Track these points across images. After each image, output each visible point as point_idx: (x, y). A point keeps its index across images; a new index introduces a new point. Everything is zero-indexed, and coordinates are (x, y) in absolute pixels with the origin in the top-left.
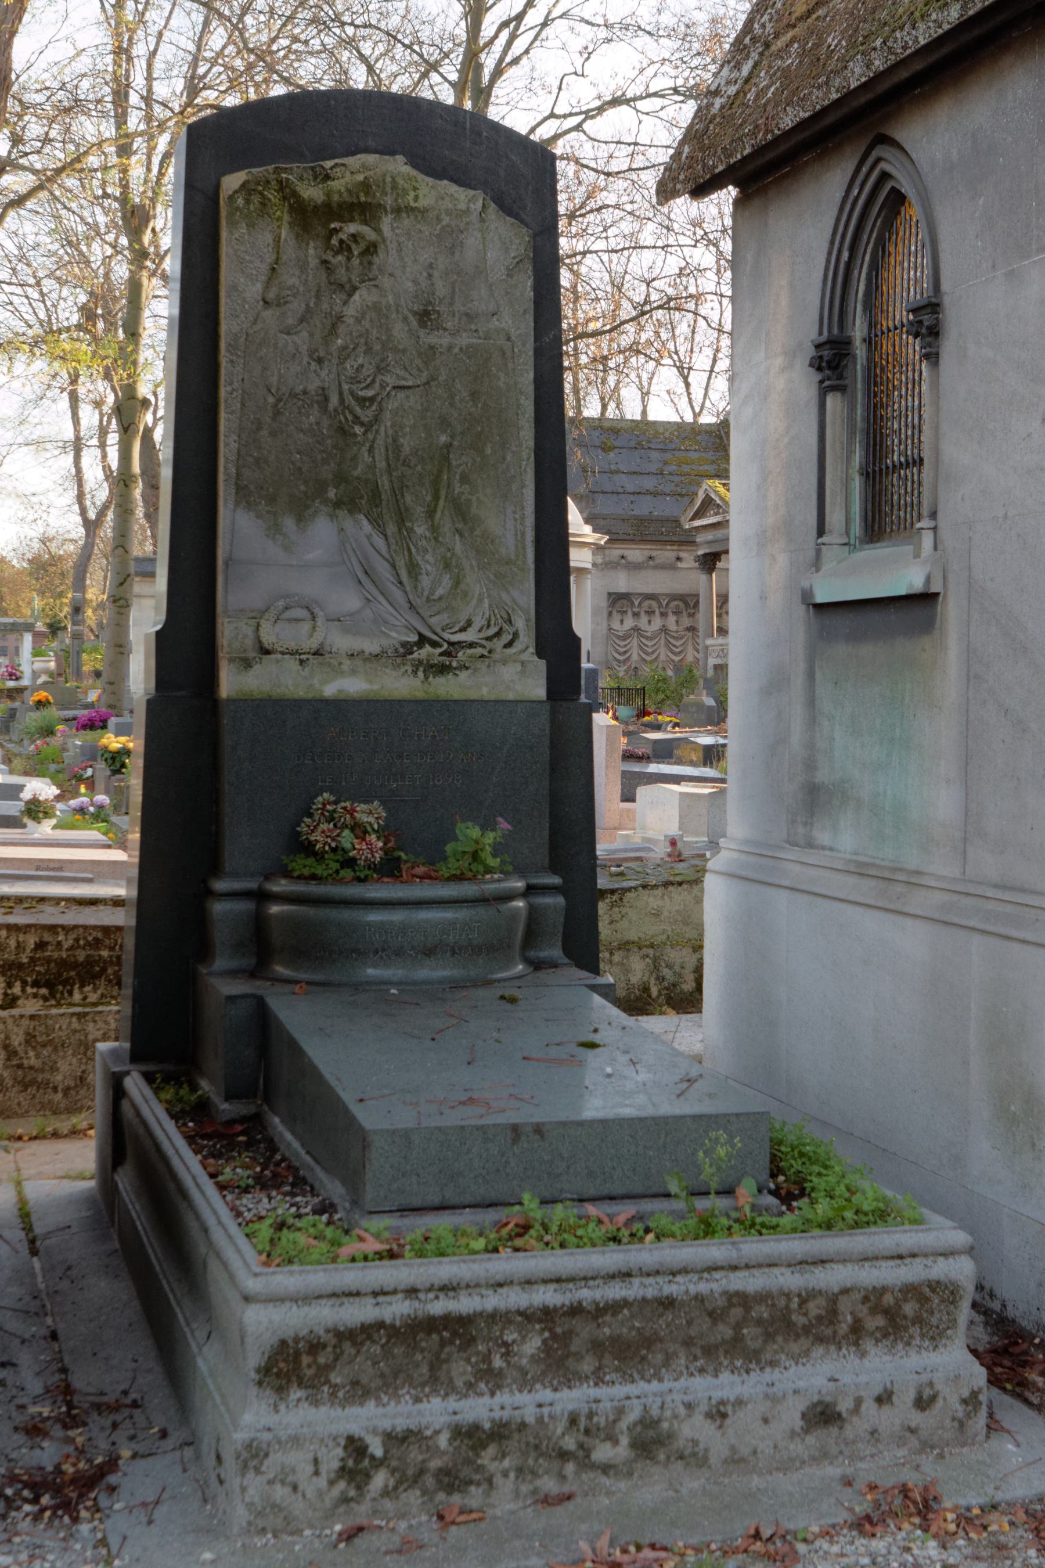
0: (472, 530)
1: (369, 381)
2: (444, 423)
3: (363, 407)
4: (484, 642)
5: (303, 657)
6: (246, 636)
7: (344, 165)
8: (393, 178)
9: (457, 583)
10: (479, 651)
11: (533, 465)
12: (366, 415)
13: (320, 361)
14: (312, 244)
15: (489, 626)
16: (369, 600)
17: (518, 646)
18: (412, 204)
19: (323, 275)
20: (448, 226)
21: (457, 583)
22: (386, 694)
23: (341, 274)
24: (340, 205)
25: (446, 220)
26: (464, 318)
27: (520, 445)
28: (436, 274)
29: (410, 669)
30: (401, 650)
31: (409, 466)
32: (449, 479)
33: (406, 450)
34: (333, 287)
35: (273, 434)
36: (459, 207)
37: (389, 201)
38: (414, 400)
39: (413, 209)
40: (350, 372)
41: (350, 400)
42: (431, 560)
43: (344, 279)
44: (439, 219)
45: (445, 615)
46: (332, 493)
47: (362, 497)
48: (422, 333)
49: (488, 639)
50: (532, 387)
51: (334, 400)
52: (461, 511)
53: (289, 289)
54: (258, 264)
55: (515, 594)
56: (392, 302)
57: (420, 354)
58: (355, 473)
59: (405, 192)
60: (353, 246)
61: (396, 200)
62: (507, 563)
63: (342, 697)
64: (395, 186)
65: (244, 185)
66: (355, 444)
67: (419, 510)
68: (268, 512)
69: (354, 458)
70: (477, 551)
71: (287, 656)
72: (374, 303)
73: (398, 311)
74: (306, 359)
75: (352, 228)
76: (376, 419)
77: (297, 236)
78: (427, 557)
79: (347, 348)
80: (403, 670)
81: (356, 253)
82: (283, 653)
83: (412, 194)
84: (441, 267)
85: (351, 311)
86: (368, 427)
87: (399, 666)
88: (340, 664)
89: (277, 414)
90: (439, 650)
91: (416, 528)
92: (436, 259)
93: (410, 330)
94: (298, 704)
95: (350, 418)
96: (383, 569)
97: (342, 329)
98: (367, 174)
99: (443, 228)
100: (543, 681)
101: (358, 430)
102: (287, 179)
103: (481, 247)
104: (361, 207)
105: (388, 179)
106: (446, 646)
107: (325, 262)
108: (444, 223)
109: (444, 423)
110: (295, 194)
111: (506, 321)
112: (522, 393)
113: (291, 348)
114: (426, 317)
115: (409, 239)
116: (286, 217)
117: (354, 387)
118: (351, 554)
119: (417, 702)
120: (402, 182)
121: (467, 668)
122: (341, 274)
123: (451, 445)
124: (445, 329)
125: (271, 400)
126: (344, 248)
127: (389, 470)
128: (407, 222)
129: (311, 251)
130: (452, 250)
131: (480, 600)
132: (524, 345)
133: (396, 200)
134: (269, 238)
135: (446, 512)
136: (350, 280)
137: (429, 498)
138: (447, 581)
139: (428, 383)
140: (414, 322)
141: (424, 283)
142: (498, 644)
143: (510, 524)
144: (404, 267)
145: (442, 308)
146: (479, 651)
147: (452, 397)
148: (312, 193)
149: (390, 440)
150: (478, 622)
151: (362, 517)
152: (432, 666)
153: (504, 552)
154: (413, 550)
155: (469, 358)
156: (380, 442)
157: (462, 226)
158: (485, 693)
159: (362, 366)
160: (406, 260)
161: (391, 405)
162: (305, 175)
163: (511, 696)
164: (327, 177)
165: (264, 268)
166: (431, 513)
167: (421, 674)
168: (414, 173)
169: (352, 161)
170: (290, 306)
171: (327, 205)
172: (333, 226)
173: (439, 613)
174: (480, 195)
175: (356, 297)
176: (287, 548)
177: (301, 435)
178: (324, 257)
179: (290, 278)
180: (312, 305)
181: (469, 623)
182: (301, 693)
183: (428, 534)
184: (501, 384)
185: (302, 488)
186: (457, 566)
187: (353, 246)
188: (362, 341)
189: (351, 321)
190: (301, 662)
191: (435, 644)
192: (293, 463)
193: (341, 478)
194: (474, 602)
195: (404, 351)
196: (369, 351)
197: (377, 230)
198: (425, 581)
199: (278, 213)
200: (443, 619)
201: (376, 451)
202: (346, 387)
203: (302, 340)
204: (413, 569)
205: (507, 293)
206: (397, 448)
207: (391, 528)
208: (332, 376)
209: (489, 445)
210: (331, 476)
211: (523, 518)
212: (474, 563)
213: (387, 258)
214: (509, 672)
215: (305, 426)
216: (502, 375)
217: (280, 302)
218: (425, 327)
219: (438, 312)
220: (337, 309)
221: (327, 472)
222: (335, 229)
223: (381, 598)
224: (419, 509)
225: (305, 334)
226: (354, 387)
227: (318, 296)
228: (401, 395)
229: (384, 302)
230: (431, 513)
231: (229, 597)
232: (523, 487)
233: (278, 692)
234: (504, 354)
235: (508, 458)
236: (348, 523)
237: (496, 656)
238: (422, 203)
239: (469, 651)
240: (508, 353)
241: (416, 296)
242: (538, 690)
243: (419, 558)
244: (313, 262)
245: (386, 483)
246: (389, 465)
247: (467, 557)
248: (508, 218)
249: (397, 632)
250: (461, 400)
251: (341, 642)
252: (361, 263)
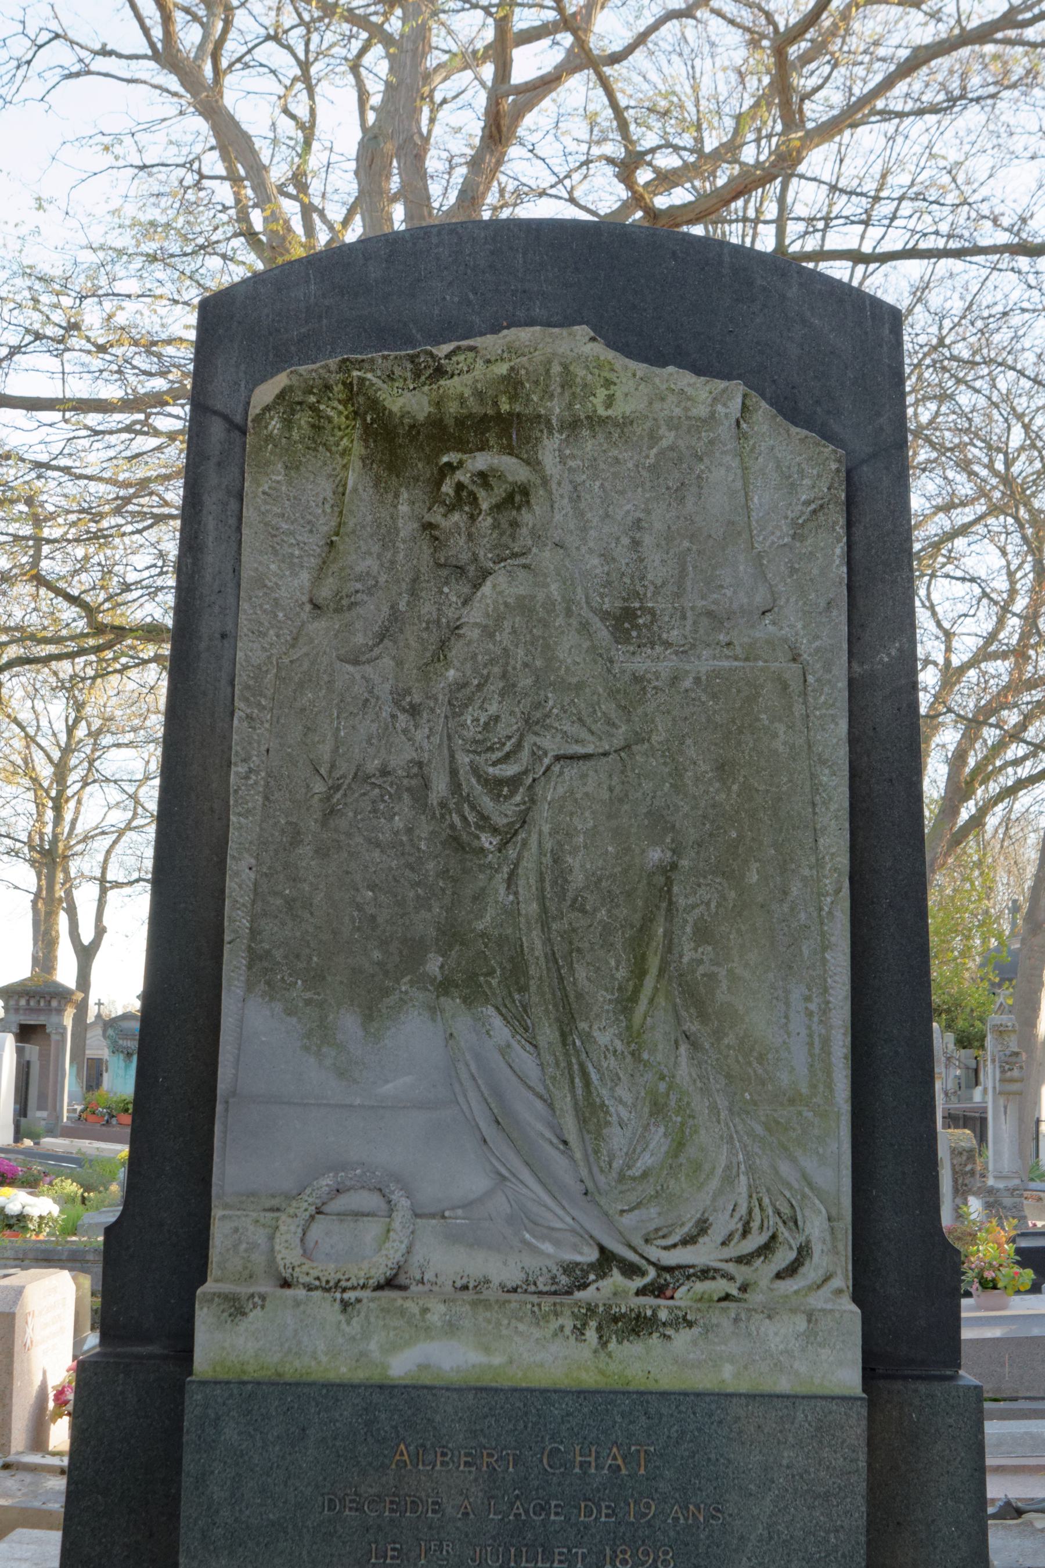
0: (718, 1035)
1: (508, 748)
2: (659, 823)
3: (497, 797)
4: (731, 1268)
5: (350, 1295)
6: (253, 1246)
7: (472, 349)
8: (566, 367)
9: (679, 1146)
10: (721, 1286)
11: (847, 904)
12: (502, 813)
13: (414, 711)
14: (405, 495)
15: (746, 1232)
16: (504, 1178)
17: (810, 1273)
18: (601, 411)
19: (426, 549)
20: (671, 448)
21: (679, 1146)
22: (516, 1377)
23: (459, 548)
24: (460, 422)
25: (668, 438)
26: (705, 621)
27: (819, 864)
28: (648, 540)
29: (569, 1324)
30: (564, 1280)
31: (583, 911)
32: (668, 934)
33: (578, 879)
34: (445, 572)
35: (322, 853)
36: (694, 412)
37: (555, 408)
38: (594, 782)
39: (603, 421)
40: (472, 732)
41: (471, 785)
42: (627, 1097)
43: (465, 557)
44: (653, 437)
45: (653, 1211)
46: (433, 965)
47: (491, 973)
48: (619, 653)
49: (739, 1260)
50: (843, 751)
51: (440, 786)
52: (693, 995)
53: (359, 579)
54: (305, 537)
55: (809, 1164)
56: (556, 595)
57: (612, 693)
58: (480, 926)
59: (589, 391)
60: (481, 494)
61: (570, 405)
62: (792, 1101)
63: (427, 1380)
64: (567, 382)
65: (281, 396)
66: (482, 868)
67: (602, 999)
68: (308, 1002)
69: (479, 897)
70: (728, 1076)
71: (317, 1294)
72: (520, 598)
73: (569, 613)
74: (387, 710)
75: (481, 461)
76: (524, 819)
77: (377, 482)
78: (620, 1091)
79: (465, 685)
80: (554, 1324)
81: (485, 506)
82: (310, 1288)
83: (602, 393)
84: (658, 525)
85: (474, 615)
86: (507, 836)
87: (545, 1317)
88: (425, 1310)
89: (330, 813)
90: (639, 1282)
91: (595, 1033)
92: (648, 512)
93: (593, 649)
94: (334, 1391)
95: (472, 818)
96: (529, 1112)
97: (457, 650)
98: (516, 362)
99: (662, 453)
100: (855, 1355)
101: (487, 841)
102: (362, 380)
103: (739, 484)
104: (504, 424)
105: (556, 369)
106: (652, 1273)
107: (428, 526)
108: (664, 443)
109: (659, 823)
110: (374, 404)
111: (792, 623)
112: (823, 762)
113: (359, 689)
114: (627, 621)
115: (595, 477)
116: (358, 449)
117: (480, 760)
118: (468, 1084)
119: (582, 1394)
120: (582, 373)
121: (690, 1324)
122: (459, 548)
123: (674, 866)
124: (667, 644)
125: (319, 787)
126: (464, 497)
127: (545, 919)
128: (590, 444)
129: (404, 508)
130: (679, 493)
131: (729, 1179)
132: (827, 667)
133: (570, 405)
134: (326, 487)
135: (661, 1001)
136: (475, 559)
137: (621, 974)
138: (658, 1139)
139: (627, 747)
140: (603, 633)
141: (623, 556)
142: (764, 1270)
143: (798, 1023)
144: (584, 529)
145: (661, 604)
146: (721, 1286)
147: (678, 773)
148: (407, 402)
149: (548, 860)
150: (723, 1224)
151: (491, 1011)
152: (615, 1319)
153: (784, 1078)
154: (594, 1076)
155: (714, 696)
156: (529, 863)
157: (700, 447)
158: (728, 1377)
159: (497, 719)
160: (586, 511)
161: (551, 792)
162: (398, 371)
163: (784, 1385)
164: (440, 372)
165: (315, 542)
166: (626, 1003)
167: (591, 1334)
168: (610, 355)
169: (489, 343)
170: (360, 610)
171: (436, 423)
172: (445, 459)
173: (639, 1205)
174: (737, 389)
175: (487, 589)
176: (342, 1073)
177: (376, 854)
178: (428, 518)
179: (362, 559)
180: (402, 606)
181: (703, 1227)
182: (342, 1370)
183: (619, 1045)
184: (778, 745)
185: (377, 955)
186: (679, 1110)
187: (481, 494)
188: (496, 670)
189: (476, 633)
190: (345, 1305)
191: (630, 1270)
192: (359, 908)
193: (452, 935)
194: (714, 1183)
195: (580, 686)
196: (509, 690)
197: (533, 463)
198: (617, 1139)
199: (345, 442)
200: (652, 1216)
201: (522, 882)
202: (463, 759)
203: (382, 673)
204: (591, 1114)
205: (793, 571)
206: (561, 876)
207: (548, 1034)
208: (436, 740)
209: (755, 866)
210: (432, 932)
211: (825, 1009)
212: (722, 1102)
213: (551, 514)
214: (780, 1333)
215: (385, 837)
216: (781, 728)
217: (343, 605)
218: (627, 641)
219: (652, 612)
220: (450, 613)
221: (424, 923)
222: (449, 464)
223: (526, 1175)
224: (602, 995)
225: (387, 662)
226: (480, 760)
227: (413, 593)
228: (572, 771)
229: (541, 597)
230: (626, 1003)
231: (232, 1171)
232: (825, 948)
233: (294, 1368)
234: (785, 686)
235: (795, 891)
236: (463, 1023)
237: (755, 1298)
238: (621, 408)
239: (700, 1287)
240: (795, 686)
241: (609, 583)
242: (845, 1375)
243: (604, 1092)
244: (407, 528)
245: (538, 944)
246: (544, 909)
247: (705, 1091)
248: (794, 430)
249: (557, 1243)
250: (697, 779)
251: (442, 1260)
252: (496, 526)
